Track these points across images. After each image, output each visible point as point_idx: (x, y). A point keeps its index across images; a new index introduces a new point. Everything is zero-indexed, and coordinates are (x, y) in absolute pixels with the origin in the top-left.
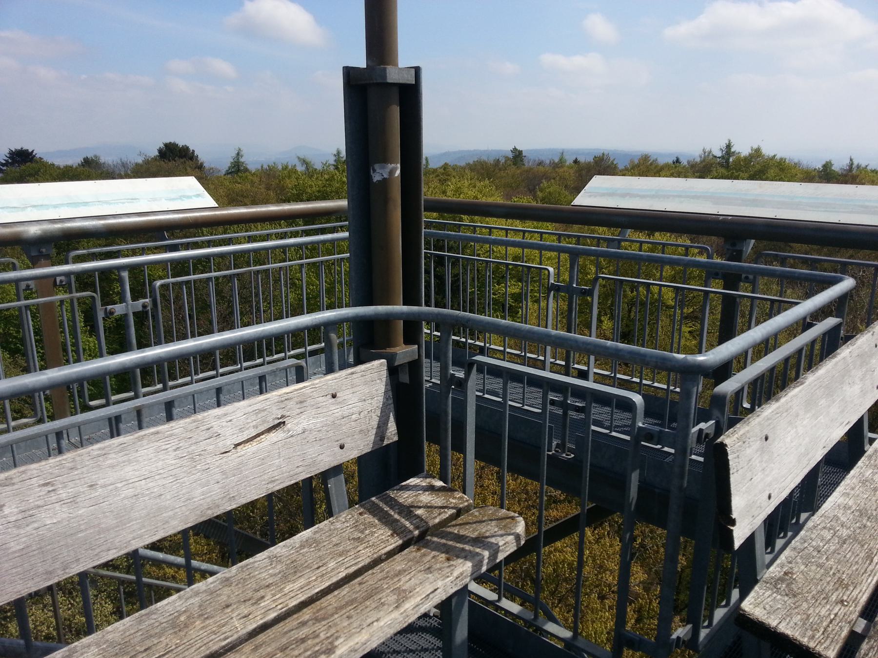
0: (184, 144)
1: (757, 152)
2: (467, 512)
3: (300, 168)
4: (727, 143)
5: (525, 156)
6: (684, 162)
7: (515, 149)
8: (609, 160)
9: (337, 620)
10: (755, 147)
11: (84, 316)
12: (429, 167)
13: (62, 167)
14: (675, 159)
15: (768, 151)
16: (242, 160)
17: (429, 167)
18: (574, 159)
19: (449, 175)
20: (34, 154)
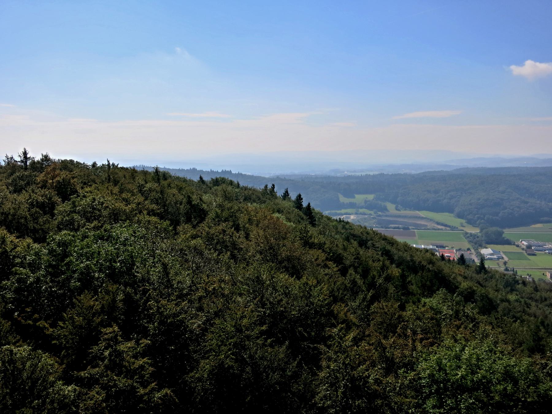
1: (46, 158)
10: (44, 154)
15: (55, 156)
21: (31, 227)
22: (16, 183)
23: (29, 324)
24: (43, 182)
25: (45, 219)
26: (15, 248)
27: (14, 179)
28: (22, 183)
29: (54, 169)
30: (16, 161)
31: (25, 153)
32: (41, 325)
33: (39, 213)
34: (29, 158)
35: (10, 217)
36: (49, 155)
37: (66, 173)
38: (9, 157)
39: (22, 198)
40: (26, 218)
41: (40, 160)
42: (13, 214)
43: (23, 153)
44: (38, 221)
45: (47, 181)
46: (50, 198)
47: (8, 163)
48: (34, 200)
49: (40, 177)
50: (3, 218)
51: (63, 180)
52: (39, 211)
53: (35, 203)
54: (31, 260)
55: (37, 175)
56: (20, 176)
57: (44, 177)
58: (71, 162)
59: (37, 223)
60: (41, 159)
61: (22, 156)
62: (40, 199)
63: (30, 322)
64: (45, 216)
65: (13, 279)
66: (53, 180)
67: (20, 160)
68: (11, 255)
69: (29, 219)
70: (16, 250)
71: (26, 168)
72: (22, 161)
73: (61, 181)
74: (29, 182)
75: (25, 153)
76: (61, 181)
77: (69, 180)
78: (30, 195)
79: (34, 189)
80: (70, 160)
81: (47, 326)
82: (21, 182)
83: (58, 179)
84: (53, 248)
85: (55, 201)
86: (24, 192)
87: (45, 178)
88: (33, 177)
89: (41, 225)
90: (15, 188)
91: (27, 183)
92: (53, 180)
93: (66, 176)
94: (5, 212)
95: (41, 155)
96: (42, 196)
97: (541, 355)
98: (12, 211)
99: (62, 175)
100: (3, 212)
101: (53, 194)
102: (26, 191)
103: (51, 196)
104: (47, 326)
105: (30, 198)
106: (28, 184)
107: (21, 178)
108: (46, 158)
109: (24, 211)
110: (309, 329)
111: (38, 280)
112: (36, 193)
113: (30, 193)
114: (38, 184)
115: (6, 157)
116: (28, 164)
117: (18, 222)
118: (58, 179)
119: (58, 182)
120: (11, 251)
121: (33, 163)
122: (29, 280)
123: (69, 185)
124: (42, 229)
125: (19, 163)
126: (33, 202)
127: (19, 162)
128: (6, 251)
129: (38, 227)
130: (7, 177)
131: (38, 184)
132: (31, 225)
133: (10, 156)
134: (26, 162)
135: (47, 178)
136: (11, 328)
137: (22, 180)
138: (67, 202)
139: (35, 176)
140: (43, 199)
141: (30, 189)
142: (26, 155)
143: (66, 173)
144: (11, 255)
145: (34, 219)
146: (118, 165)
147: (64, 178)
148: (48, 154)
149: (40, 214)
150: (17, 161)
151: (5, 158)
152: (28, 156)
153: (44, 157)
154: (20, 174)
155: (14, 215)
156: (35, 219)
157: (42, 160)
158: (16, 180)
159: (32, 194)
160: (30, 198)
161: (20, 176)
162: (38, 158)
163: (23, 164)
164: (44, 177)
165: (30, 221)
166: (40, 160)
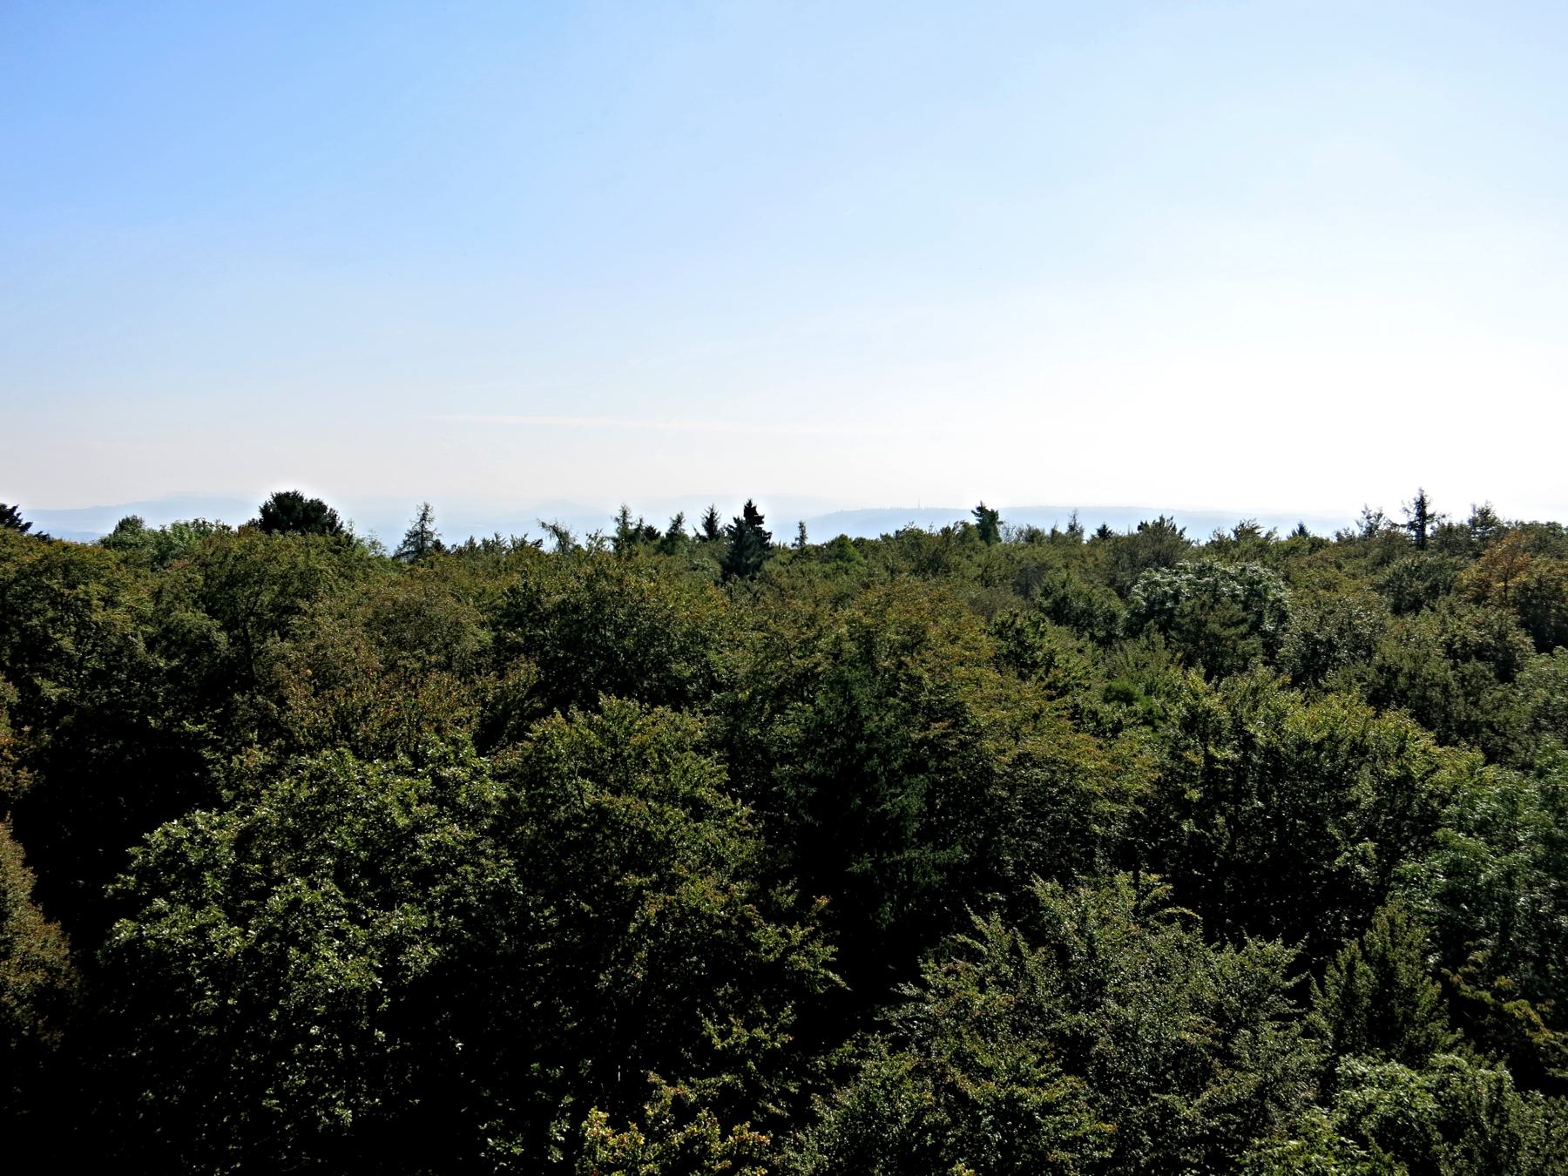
0: (315, 498)
1: (1484, 518)
2: (829, 1104)
3: (550, 545)
4: (1418, 497)
5: (1002, 523)
6: (780, 533)
7: (981, 509)
8: (1174, 529)
9: (1122, 658)
10: (1480, 505)
11: (599, 700)
12: (807, 542)
13: (1199, 536)
14: (1297, 528)
15: (1509, 512)
16: (429, 527)
17: (807, 542)
18: (1099, 526)
19: (849, 561)
20: (15, 514)
21: (1459, 714)
22: (1400, 586)
23: (1481, 999)
24: (1479, 587)
25: (1499, 695)
26: (1433, 771)
27: (1395, 574)
28: (1419, 586)
29: (1513, 550)
30: (1395, 525)
31: (1421, 504)
32: (1517, 1013)
33: (1484, 677)
34: (1432, 516)
35: (1401, 680)
36: (1493, 509)
37: (1547, 563)
38: (1372, 514)
39: (1425, 626)
40: (1446, 688)
41: (1466, 523)
42: (1410, 673)
43: (1417, 503)
44: (1478, 700)
45: (1488, 586)
46: (1501, 636)
47: (1371, 530)
48: (1455, 636)
49: (1470, 572)
50: (1383, 683)
51: (1539, 581)
52: (1482, 671)
53: (1457, 646)
54: (1489, 815)
55: (1458, 566)
56: (1413, 565)
57: (1481, 571)
58: (1551, 528)
59: (1475, 704)
60: (1469, 521)
61: (1411, 510)
62: (1474, 636)
63: (1487, 995)
64: (1501, 687)
65: (1437, 861)
66: (1505, 581)
67: (1406, 523)
68: (1423, 791)
69: (1453, 689)
70: (1436, 777)
71: (1422, 542)
72: (1412, 526)
73: (1533, 585)
74: (1437, 585)
75: (1421, 504)
76: (1533, 585)
77: (1557, 584)
78: (1444, 622)
79: (1455, 604)
80: (1549, 524)
81: (1535, 1018)
82: (1416, 583)
83: (1522, 577)
84: (1556, 788)
85: (1517, 645)
86: (1426, 611)
87: (1483, 574)
88: (1450, 571)
89: (1487, 713)
90: (1396, 599)
91: (1430, 587)
92: (1505, 581)
93: (1549, 571)
94: (1389, 668)
95: (1471, 509)
96: (1477, 627)
97: (679, 1143)
98: (1407, 665)
99: (1537, 566)
100: (1383, 666)
101: (1509, 622)
102: (1433, 609)
103: (1504, 628)
104: (1535, 1018)
105: (1444, 631)
106: (1433, 591)
107: (1412, 572)
108: (1484, 518)
109: (1439, 668)
110: (790, 1002)
111: (1509, 876)
112: (1460, 618)
113: (1444, 616)
114: (1461, 591)
115: (1364, 513)
116: (1428, 532)
117: (1423, 698)
118: (1522, 577)
119: (1525, 588)
120: (1422, 780)
121: (1448, 531)
122: (1484, 872)
123: (1555, 598)
124: (1490, 725)
125: (1404, 531)
126: (1454, 643)
127: (1403, 526)
128: (1409, 776)
129: (1476, 714)
130: (1369, 568)
131: (1461, 591)
132: (1459, 708)
133: (1374, 511)
134: (1422, 528)
135: (1490, 575)
136: (1440, 1002)
137: (1417, 579)
138: (1562, 651)
139: (1455, 568)
140: (1482, 636)
141: (1442, 603)
142: (1425, 507)
143: (1547, 563)
144: (1423, 791)
145: (1467, 694)
146: (14, 508)
147: (1541, 576)
148: (1489, 505)
149: (1486, 679)
150: (1399, 523)
151: (1360, 517)
152: (1429, 511)
153: (1477, 515)
154: (1413, 562)
155: (1412, 677)
156: (1472, 694)
157: (1473, 522)
158: (1400, 578)
159: (1449, 620)
160: (1444, 631)
161: (1413, 565)
162: (1460, 515)
163: (1413, 533)
164: (1481, 571)
165: (1458, 696)
166: (1466, 523)
